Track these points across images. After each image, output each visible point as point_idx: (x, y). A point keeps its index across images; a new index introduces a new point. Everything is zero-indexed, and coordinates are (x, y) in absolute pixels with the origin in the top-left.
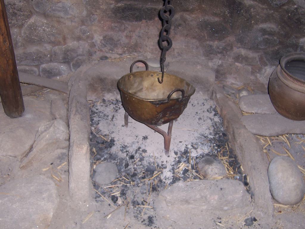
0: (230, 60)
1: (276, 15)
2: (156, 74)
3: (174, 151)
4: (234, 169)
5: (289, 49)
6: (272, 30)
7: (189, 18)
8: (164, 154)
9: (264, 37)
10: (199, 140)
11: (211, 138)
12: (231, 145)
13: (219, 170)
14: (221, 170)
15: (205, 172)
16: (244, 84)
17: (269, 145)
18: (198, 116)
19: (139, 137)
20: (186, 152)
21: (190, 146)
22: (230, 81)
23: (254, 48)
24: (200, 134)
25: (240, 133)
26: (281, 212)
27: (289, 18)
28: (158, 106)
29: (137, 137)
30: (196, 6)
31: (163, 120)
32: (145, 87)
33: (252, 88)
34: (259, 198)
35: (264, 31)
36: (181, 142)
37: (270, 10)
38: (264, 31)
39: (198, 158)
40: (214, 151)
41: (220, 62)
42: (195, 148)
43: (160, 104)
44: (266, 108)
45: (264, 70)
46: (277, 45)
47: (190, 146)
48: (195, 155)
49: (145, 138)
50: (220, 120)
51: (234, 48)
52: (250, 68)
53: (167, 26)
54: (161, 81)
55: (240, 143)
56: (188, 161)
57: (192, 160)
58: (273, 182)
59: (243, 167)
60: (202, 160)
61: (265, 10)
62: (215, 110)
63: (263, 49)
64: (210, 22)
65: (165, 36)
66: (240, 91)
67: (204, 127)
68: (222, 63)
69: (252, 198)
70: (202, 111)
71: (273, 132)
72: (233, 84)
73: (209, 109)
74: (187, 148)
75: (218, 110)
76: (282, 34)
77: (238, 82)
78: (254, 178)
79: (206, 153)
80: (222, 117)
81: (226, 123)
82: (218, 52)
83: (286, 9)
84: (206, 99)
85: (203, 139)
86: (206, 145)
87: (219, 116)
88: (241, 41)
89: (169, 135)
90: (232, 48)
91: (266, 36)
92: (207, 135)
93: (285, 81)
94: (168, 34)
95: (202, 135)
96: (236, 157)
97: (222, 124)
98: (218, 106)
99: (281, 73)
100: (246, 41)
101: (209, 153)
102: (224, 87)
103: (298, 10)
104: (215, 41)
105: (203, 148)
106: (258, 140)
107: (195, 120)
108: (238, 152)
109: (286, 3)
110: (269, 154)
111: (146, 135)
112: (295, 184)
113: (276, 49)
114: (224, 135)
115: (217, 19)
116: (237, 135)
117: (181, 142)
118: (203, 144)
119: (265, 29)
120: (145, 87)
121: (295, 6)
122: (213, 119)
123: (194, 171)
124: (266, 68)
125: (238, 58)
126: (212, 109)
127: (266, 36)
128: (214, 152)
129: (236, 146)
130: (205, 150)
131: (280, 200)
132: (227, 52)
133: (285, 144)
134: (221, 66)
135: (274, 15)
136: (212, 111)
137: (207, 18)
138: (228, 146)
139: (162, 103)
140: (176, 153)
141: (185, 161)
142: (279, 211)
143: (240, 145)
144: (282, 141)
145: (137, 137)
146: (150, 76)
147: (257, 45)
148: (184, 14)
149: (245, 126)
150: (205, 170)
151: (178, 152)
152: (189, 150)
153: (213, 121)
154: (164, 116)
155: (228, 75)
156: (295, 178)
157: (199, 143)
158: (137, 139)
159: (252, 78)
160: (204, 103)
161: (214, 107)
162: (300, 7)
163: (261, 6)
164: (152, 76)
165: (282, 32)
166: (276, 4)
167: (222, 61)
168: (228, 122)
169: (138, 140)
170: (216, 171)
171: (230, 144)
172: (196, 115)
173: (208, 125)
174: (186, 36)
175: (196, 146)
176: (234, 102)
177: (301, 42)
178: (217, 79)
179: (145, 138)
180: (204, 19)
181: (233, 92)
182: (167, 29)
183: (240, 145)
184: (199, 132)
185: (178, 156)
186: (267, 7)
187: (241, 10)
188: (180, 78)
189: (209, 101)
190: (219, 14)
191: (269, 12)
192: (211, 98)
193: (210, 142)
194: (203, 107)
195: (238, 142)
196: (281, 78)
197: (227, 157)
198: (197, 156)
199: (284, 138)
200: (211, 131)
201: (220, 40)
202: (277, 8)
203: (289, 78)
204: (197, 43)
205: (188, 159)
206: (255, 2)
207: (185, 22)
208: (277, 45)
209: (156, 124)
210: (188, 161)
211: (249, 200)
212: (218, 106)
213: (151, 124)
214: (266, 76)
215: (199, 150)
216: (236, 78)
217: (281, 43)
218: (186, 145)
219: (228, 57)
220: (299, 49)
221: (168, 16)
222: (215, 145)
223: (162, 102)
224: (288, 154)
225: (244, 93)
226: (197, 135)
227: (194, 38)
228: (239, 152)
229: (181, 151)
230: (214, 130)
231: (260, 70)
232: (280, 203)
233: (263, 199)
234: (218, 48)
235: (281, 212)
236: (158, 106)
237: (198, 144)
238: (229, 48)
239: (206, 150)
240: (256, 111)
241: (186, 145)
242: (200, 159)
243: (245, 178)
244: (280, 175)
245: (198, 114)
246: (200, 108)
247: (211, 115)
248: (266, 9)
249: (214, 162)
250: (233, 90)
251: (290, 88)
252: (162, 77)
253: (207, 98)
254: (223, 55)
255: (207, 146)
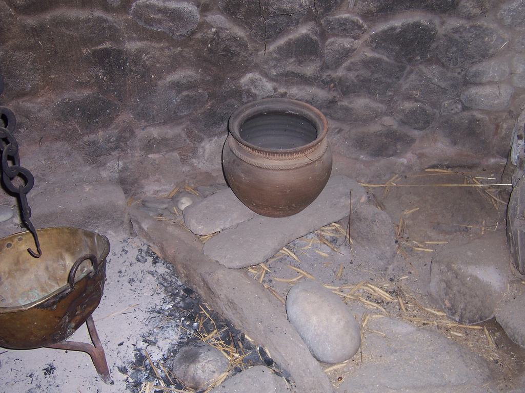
0: (138, 154)
1: (188, 52)
2: (16, 240)
3: (118, 368)
4: (236, 346)
5: (229, 101)
6: (189, 79)
7: (34, 107)
8: (101, 383)
9: (180, 95)
10: (151, 323)
11: (169, 308)
12: (211, 306)
13: (215, 363)
14: (217, 361)
15: (193, 378)
16: (177, 185)
17: (267, 272)
18: (124, 278)
19: (36, 374)
20: (141, 359)
21: (141, 345)
22: (150, 189)
23: (172, 119)
24: (147, 310)
25: (218, 280)
26: (341, 378)
27: (210, 51)
28: (55, 306)
29: (30, 376)
30: (38, 81)
31: (73, 325)
32: (4, 273)
33: (193, 185)
34: (302, 377)
35: (177, 86)
36: (121, 344)
37: (174, 46)
38: (177, 86)
39: (167, 358)
40: (188, 332)
41: (121, 163)
42: (154, 343)
43: (59, 301)
44: (235, 215)
45: (201, 150)
46: (207, 101)
47: (141, 345)
48: (160, 357)
49: (49, 370)
50: (169, 268)
51: (137, 131)
52: (176, 155)
53: (9, 149)
54: (38, 254)
55: (226, 297)
56: (152, 375)
57: (160, 368)
58: (309, 337)
59: (248, 336)
60: (176, 359)
61: (167, 50)
62: (149, 253)
63: (187, 115)
64: (76, 101)
65: (11, 168)
66: (174, 199)
67: (147, 293)
68: (125, 164)
69: (288, 381)
70: (127, 264)
71: (268, 252)
72: (160, 191)
73: (139, 257)
74: (139, 350)
75: (156, 250)
76: (208, 81)
77: (164, 185)
78: (277, 347)
79: (175, 342)
80: (170, 263)
81: (182, 270)
82: (111, 148)
83: (200, 38)
84: (124, 241)
85: (158, 319)
86: (168, 327)
87: (163, 262)
88: (144, 115)
89: (97, 346)
90: (132, 133)
91: (185, 93)
92: (160, 307)
93: (253, 161)
94: (16, 162)
95: (152, 311)
96: (228, 323)
97: (175, 273)
98: (151, 245)
99: (240, 149)
100: (153, 112)
101: (181, 338)
102: (144, 204)
103: (220, 34)
104: (98, 132)
105: (167, 335)
106: (246, 273)
107: (123, 287)
108: (229, 314)
109: (196, 29)
110: (273, 288)
111: (49, 362)
112: (342, 323)
113: (208, 109)
114: (189, 291)
115: (86, 93)
116: (214, 287)
117: (121, 344)
118: (163, 328)
119: (178, 83)
120: (4, 273)
121: (213, 30)
122: (156, 271)
123: (172, 387)
124: (203, 144)
125: (150, 146)
126: (143, 254)
127: (185, 93)
128: (190, 334)
129: (221, 304)
130: (172, 338)
131: (331, 360)
132: (126, 143)
133: (288, 259)
134: (125, 169)
135: (184, 54)
136: (147, 258)
137: (66, 96)
138: (206, 309)
139: (62, 298)
140: (123, 370)
141: (148, 378)
142: (338, 379)
143: (229, 301)
144: (282, 256)
145: (30, 376)
146: (6, 248)
147: (175, 112)
148: (20, 103)
149: (217, 261)
150: (192, 375)
151: (127, 365)
152: (144, 354)
153: (157, 275)
154: (73, 316)
155: (143, 181)
156: (338, 314)
157: (155, 330)
158: (34, 379)
159: (186, 169)
160: (126, 249)
161: (145, 248)
162: (221, 28)
163: (157, 45)
164: (9, 245)
165: (208, 78)
166: (180, 35)
167: (125, 160)
168: (185, 267)
169: (37, 382)
170: (211, 367)
171: (206, 304)
172: (120, 276)
173: (150, 287)
174: (40, 141)
175: (152, 338)
176: (176, 225)
177: (243, 85)
178: (126, 195)
179: (49, 370)
180: (64, 100)
181: (165, 206)
182: (11, 154)
183: (229, 301)
184: (144, 306)
185: (129, 373)
186: (167, 44)
187: (125, 63)
188: (68, 228)
189: (130, 240)
190: (89, 82)
191: (175, 52)
192: (133, 234)
193: (172, 317)
194: (125, 256)
195: (222, 296)
196: (244, 158)
197: (215, 331)
198: (164, 355)
199: (284, 250)
200: (163, 295)
201: (106, 126)
202: (184, 40)
203: (257, 153)
204: (67, 145)
205: (151, 369)
206: (145, 42)
207: (27, 117)
208: (207, 101)
209: (64, 336)
210: (152, 375)
211: (286, 387)
212: (151, 245)
213: (55, 341)
214: (208, 159)
215: (160, 343)
216: (158, 181)
217: (211, 96)
218: (134, 345)
219: (131, 150)
220: (244, 96)
221: (4, 128)
222: (183, 319)
223: (60, 295)
224: (303, 274)
225: (185, 203)
226: (142, 316)
227: (56, 140)
228: (230, 313)
229: (130, 360)
230: (166, 290)
231: (194, 151)
232: (332, 364)
233: (308, 375)
234: (109, 141)
235: (341, 378)
236: (55, 306)
237: (154, 332)
238: (128, 135)
239: (170, 337)
240: (222, 227)
241: (134, 345)
242: (172, 358)
243: (262, 352)
244: (314, 320)
245: (123, 273)
246: (121, 260)
247: (148, 265)
248: (168, 48)
249: (201, 354)
250: (163, 203)
251: (267, 169)
252: (37, 245)
253: (125, 236)
254: (122, 151)
255: (171, 328)
